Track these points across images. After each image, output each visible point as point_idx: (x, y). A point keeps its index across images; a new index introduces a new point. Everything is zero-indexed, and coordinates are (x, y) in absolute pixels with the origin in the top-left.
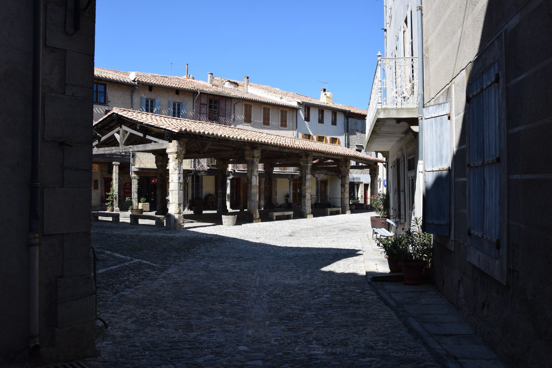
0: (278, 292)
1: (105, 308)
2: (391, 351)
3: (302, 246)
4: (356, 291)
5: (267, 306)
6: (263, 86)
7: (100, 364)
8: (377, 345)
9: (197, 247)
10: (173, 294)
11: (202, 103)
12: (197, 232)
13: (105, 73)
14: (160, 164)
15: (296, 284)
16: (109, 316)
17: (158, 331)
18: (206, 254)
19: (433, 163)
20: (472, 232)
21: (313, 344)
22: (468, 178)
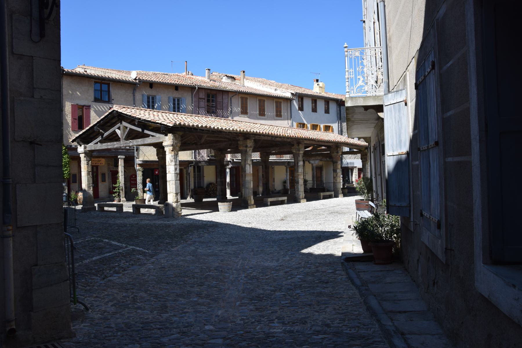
0: (255, 274)
2: (346, 328)
3: (289, 230)
4: (328, 272)
6: (259, 79)
7: (73, 344)
8: (334, 322)
9: (190, 233)
10: (157, 278)
12: (194, 219)
13: (109, 73)
14: (161, 157)
15: (275, 266)
16: (92, 300)
17: (135, 313)
19: (393, 147)
20: (424, 213)
21: (275, 322)
22: (419, 161)
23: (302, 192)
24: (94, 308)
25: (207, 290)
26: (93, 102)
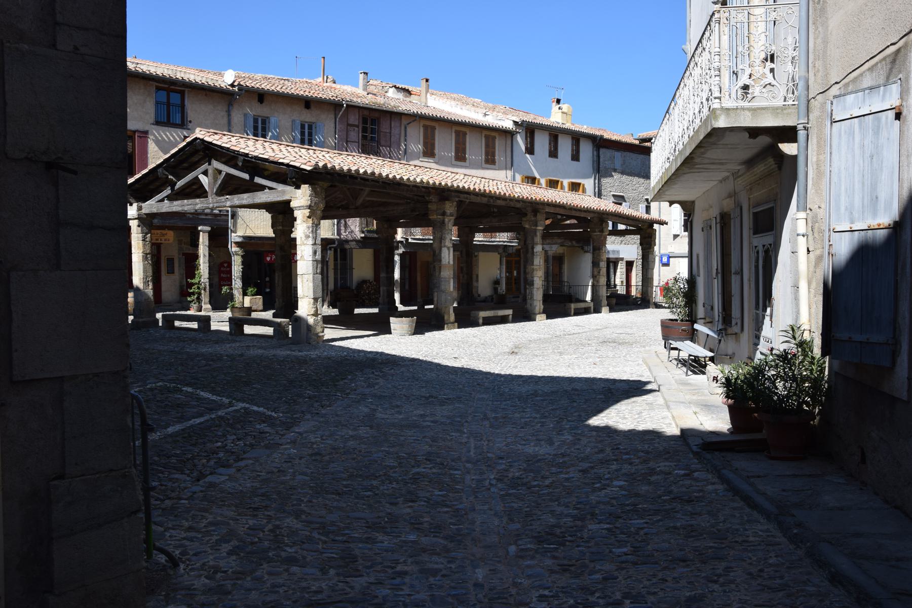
0: (517, 474)
1: (175, 516)
4: (677, 473)
5: (502, 505)
11: (351, 123)
12: (348, 348)
14: (280, 230)
18: (367, 391)
23: (540, 301)
24: (188, 560)
25: (430, 512)
26: (153, 124)
